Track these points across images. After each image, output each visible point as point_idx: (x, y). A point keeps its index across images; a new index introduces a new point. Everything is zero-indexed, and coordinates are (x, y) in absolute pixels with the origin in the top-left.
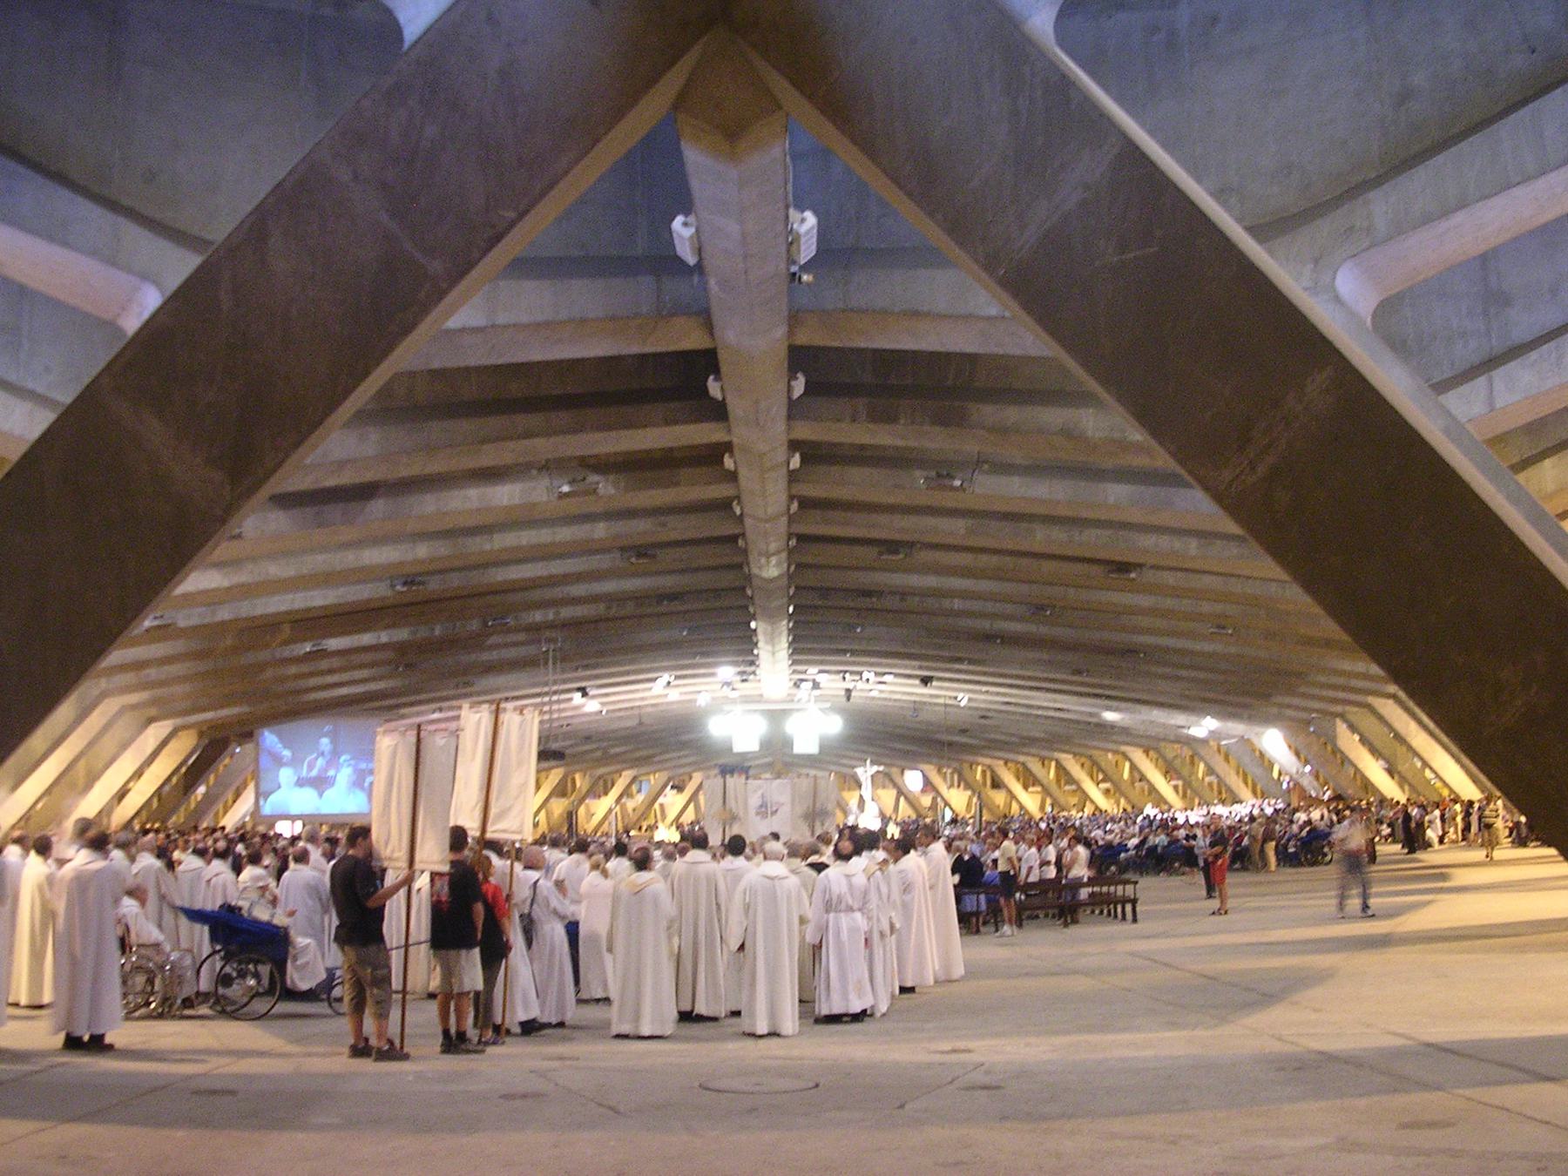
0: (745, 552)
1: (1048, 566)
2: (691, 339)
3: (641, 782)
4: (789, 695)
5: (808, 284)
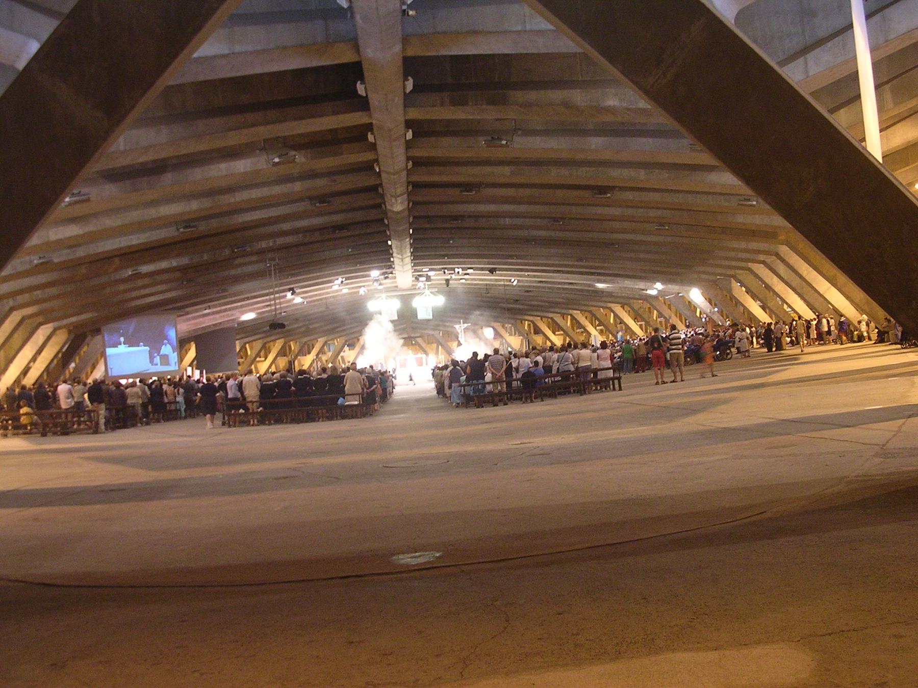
0: (382, 196)
1: (560, 193)
2: (348, 57)
3: (329, 344)
4: (413, 285)
5: (412, 16)
